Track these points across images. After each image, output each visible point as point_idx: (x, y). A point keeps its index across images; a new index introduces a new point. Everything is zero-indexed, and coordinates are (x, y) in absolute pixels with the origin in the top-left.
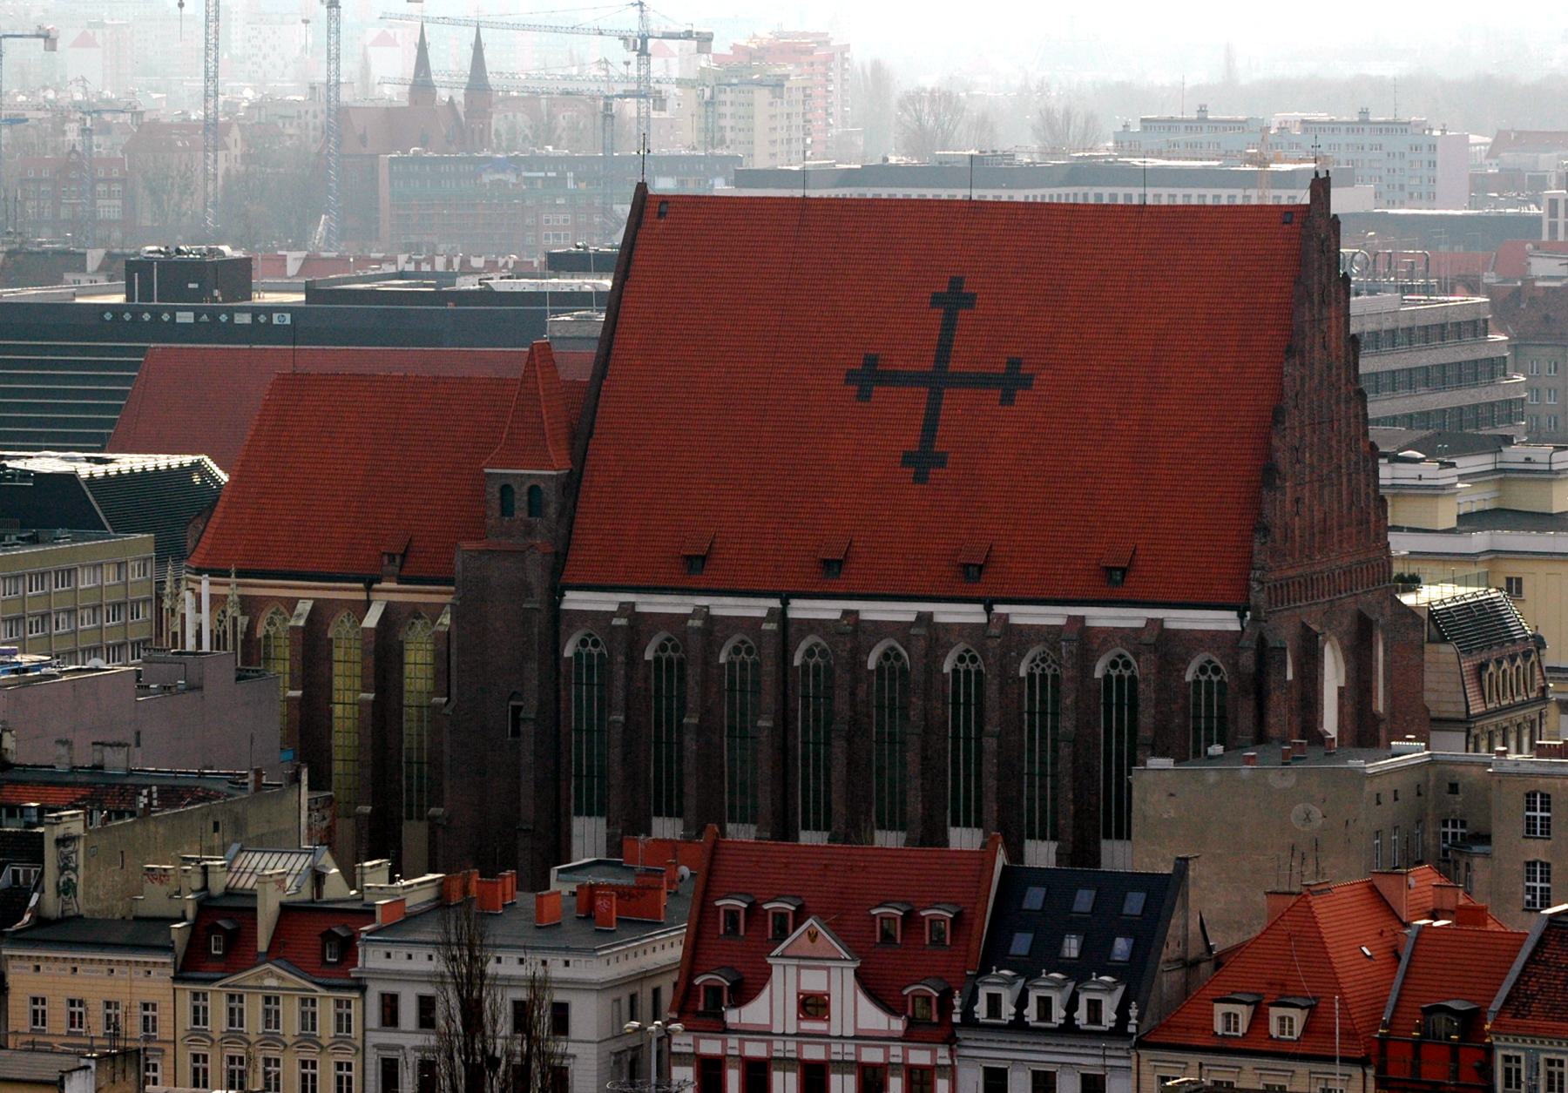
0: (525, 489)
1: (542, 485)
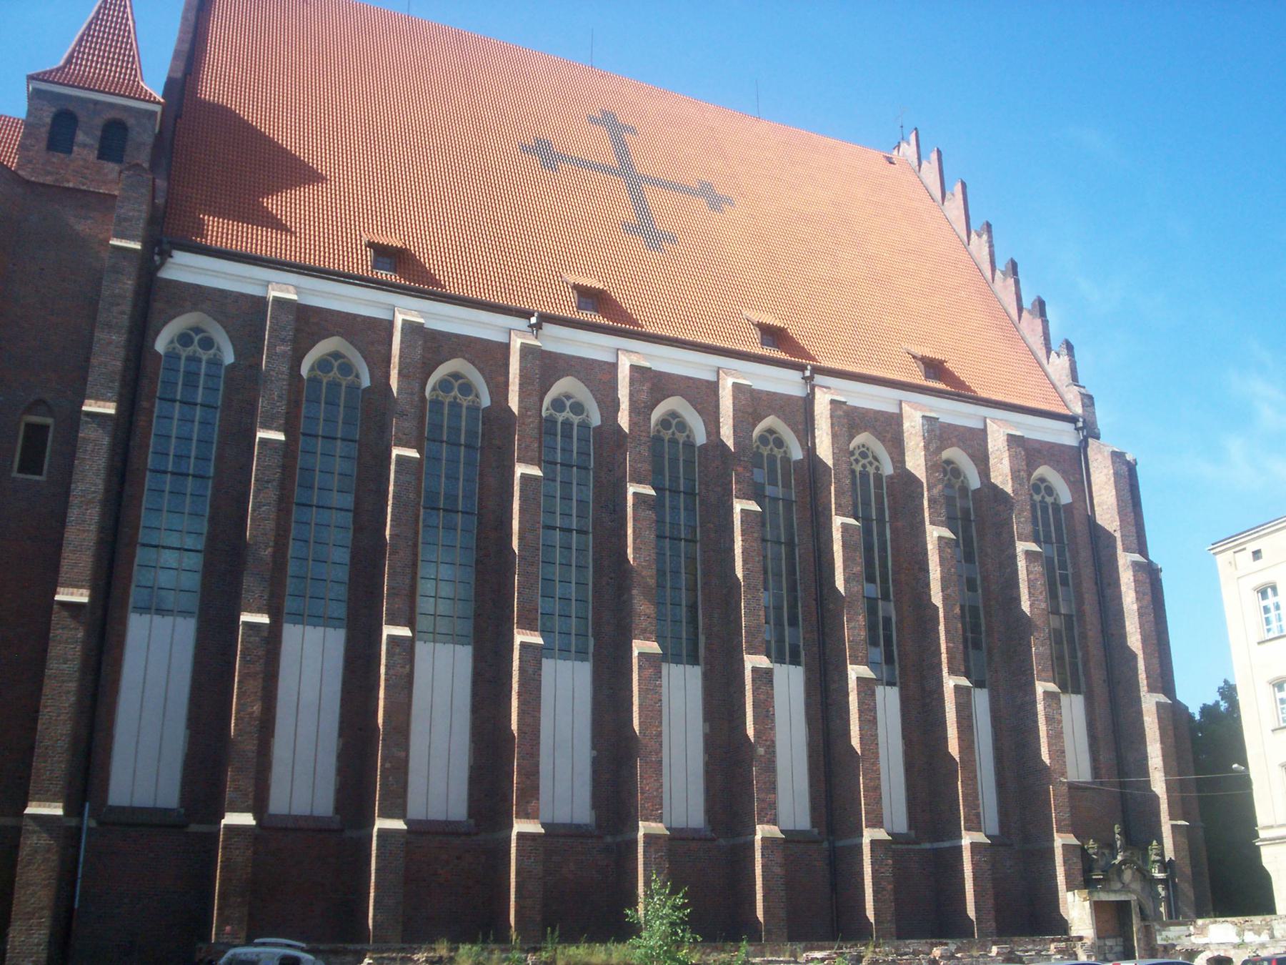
0: (99, 122)
1: (131, 122)
